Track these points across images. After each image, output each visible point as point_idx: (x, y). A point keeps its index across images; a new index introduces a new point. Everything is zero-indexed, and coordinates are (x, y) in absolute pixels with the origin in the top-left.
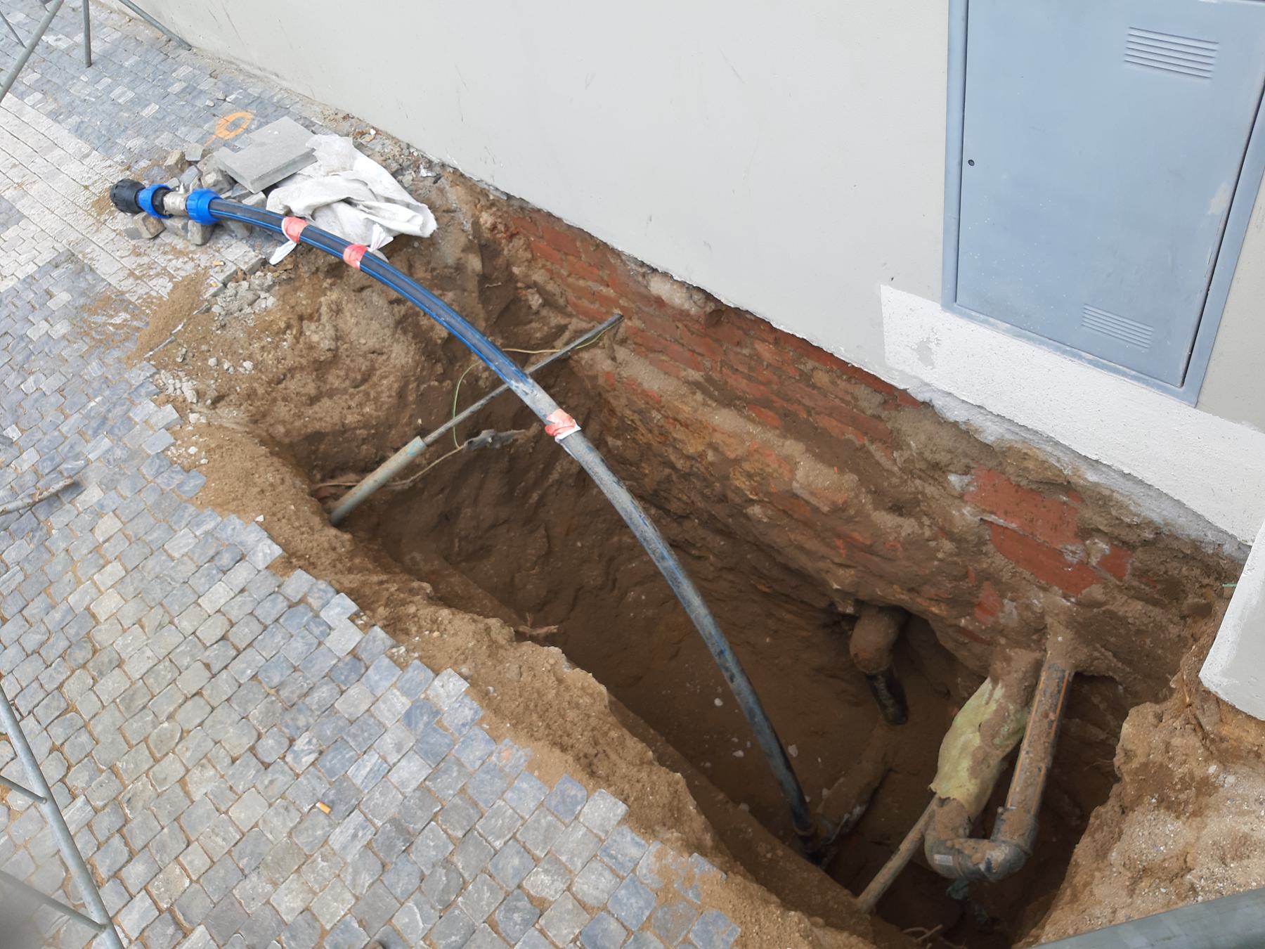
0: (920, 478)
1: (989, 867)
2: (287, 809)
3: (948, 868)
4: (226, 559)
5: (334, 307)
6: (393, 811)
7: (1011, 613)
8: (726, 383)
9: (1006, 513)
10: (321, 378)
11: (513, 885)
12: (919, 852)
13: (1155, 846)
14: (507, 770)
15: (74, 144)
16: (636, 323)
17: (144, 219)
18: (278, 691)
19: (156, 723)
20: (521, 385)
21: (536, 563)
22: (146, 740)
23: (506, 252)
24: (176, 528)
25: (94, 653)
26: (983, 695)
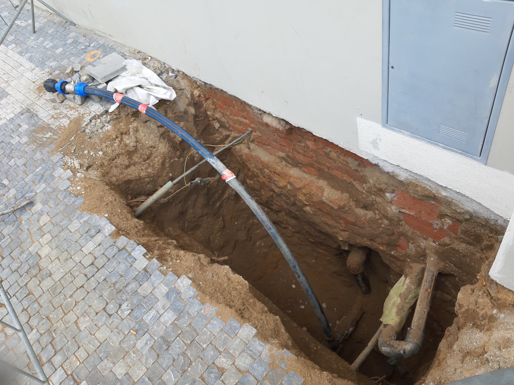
0: (374, 195)
1: (404, 352)
2: (119, 333)
3: (388, 353)
4: (93, 232)
5: (135, 129)
6: (162, 333)
9: (409, 208)
10: (130, 158)
11: (211, 363)
13: (472, 343)
14: (208, 316)
15: (29, 65)
16: (258, 133)
17: (57, 95)
18: (114, 285)
19: (65, 299)
20: (211, 160)
21: (219, 231)
22: (61, 306)
23: (204, 106)
24: (72, 219)
25: (40, 270)
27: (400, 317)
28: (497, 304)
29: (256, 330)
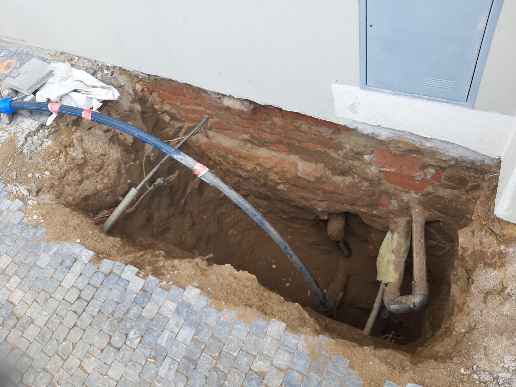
0: (351, 159)
1: (414, 306)
2: (134, 365)
3: (397, 310)
4: (68, 263)
5: (79, 139)
6: (184, 353)
7: (395, 205)
8: (261, 137)
9: (390, 166)
11: (247, 370)
12: (382, 306)
13: (489, 282)
14: (229, 322)
16: (216, 119)
18: (113, 315)
19: (59, 343)
20: (179, 156)
21: (189, 229)
22: (56, 352)
23: (150, 100)
24: (39, 254)
25: (18, 319)
26: (389, 239)
27: (398, 273)
28: (503, 240)
29: (285, 324)
